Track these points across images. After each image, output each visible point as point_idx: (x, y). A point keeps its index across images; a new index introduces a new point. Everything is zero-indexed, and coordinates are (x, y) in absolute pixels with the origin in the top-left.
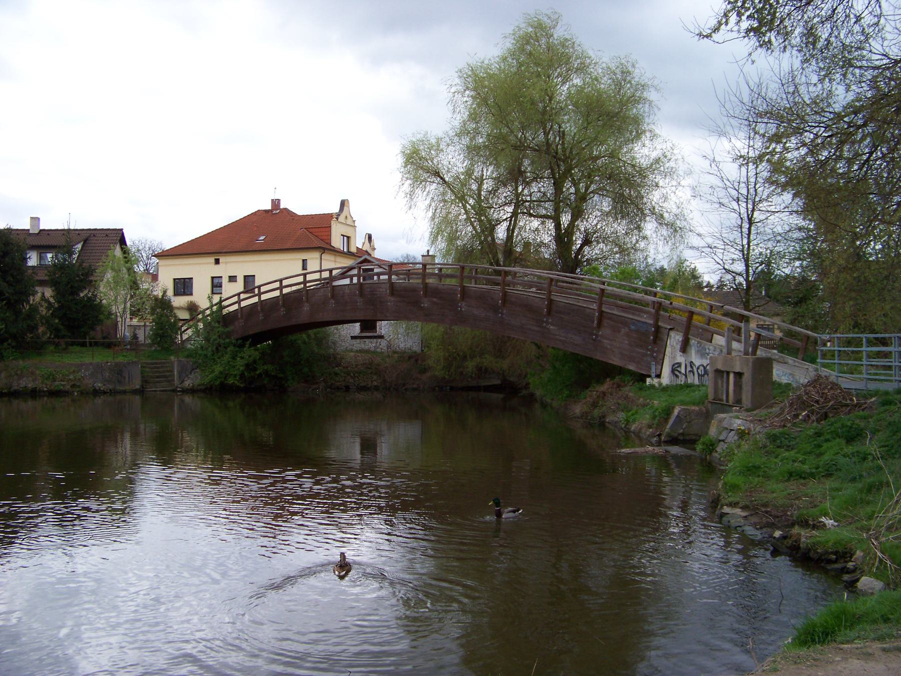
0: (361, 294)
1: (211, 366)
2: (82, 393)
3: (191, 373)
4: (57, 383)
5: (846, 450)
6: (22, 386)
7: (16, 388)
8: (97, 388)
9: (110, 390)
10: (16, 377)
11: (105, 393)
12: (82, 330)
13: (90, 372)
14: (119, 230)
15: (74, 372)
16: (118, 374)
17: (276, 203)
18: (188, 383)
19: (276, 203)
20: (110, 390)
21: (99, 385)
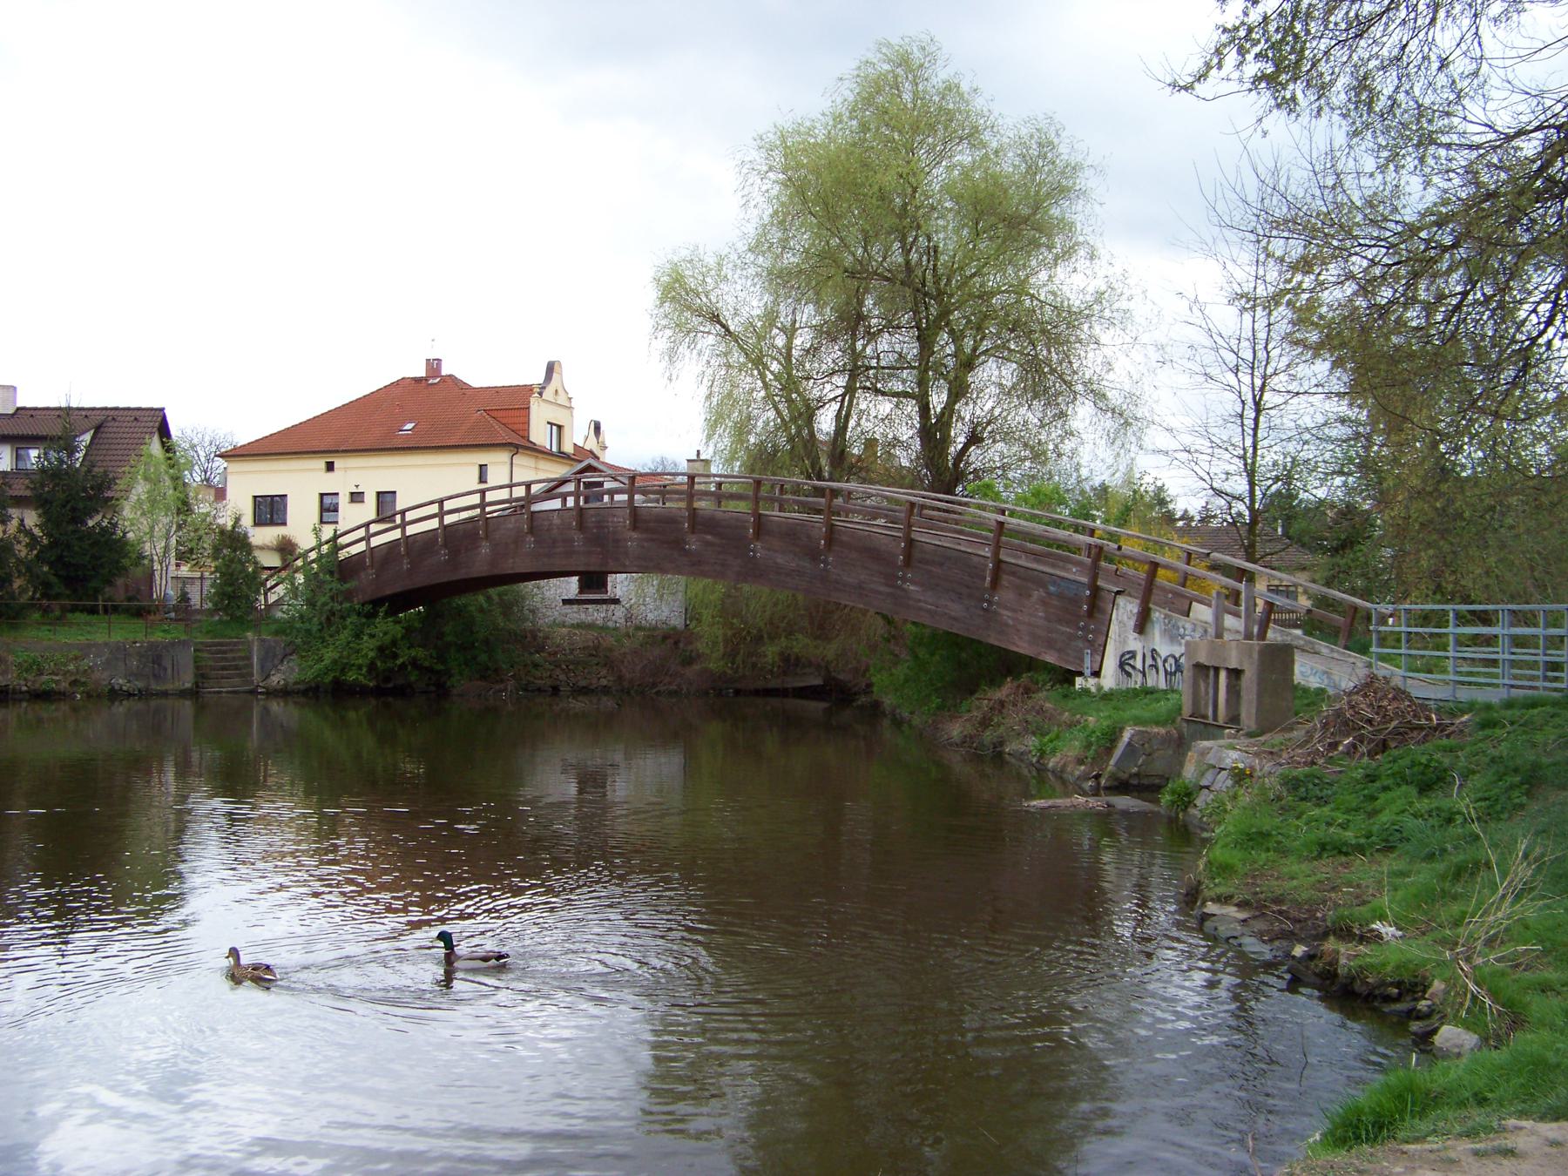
3: (282, 661)
4: (45, 678)
8: (117, 687)
9: (140, 691)
11: (130, 695)
20: (140, 691)
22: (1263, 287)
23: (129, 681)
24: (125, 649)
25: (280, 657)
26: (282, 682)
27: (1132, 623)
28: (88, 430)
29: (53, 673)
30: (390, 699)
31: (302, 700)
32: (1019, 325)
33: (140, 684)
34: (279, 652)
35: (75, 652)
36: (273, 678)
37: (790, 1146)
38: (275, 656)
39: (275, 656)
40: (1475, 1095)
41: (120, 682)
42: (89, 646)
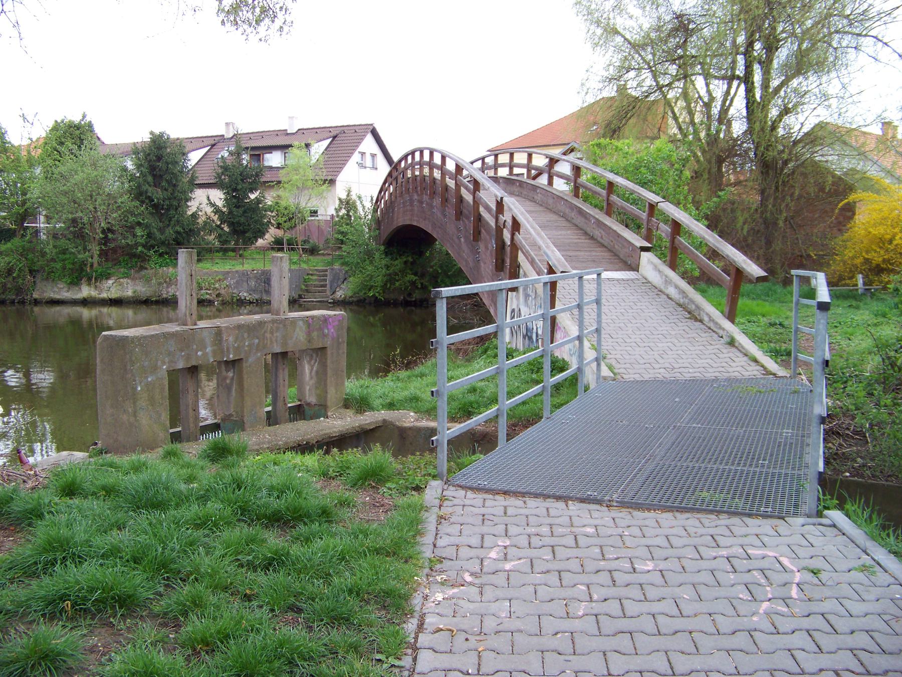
0: (260, 231)
1: (756, 225)
2: (224, 303)
3: (343, 282)
4: (203, 291)
5: (200, 534)
6: (170, 294)
7: (165, 296)
8: (243, 298)
9: (257, 300)
10: (165, 285)
11: (251, 303)
12: (247, 235)
13: (235, 281)
14: (221, 136)
15: (219, 280)
16: (265, 283)
17: (152, 133)
18: (340, 294)
19: (152, 133)
20: (257, 300)
21: (245, 294)
22: (667, 82)
23: (250, 294)
24: (247, 275)
25: (342, 280)
26: (343, 296)
27: (454, 218)
28: (328, 138)
29: (207, 289)
30: (413, 308)
31: (355, 308)
32: (621, 94)
33: (256, 296)
34: (342, 276)
35: (221, 277)
36: (338, 293)
37: (228, 381)
38: (339, 279)
39: (339, 279)
40: (54, 234)
41: (244, 295)
42: (228, 273)
